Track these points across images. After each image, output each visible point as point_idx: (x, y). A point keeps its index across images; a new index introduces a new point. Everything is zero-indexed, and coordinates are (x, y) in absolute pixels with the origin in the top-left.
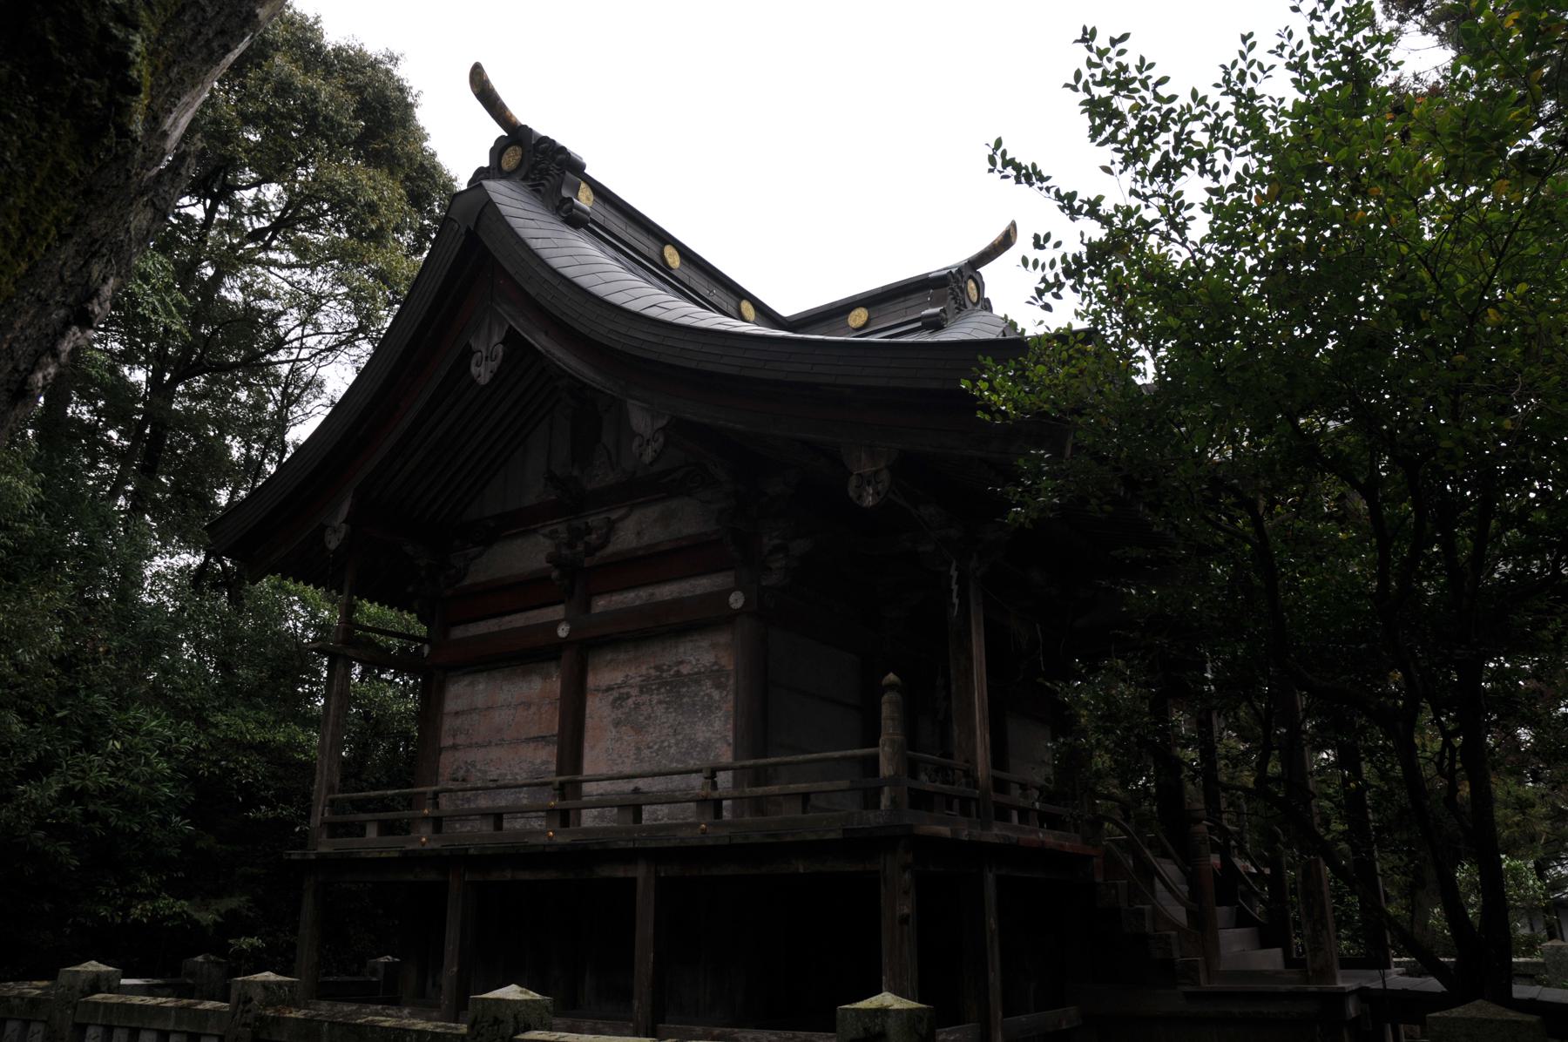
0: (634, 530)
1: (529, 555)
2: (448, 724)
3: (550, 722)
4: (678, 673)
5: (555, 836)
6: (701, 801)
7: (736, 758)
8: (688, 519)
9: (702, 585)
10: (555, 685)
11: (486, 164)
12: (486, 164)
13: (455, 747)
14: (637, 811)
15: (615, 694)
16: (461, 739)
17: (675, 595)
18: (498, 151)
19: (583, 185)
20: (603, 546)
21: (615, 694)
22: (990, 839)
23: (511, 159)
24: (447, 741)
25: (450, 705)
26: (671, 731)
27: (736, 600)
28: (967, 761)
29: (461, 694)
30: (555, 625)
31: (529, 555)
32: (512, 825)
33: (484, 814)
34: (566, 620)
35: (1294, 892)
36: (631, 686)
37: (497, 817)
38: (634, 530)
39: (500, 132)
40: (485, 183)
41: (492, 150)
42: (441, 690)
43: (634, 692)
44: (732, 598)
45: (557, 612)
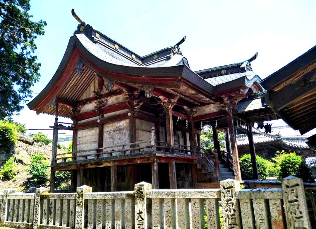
0: (112, 100)
1: (90, 107)
2: (78, 140)
3: (97, 138)
4: (120, 128)
5: (220, 217)
6: (122, 151)
7: (256, 144)
8: (121, 98)
9: (124, 111)
10: (210, 93)
11: (77, 30)
12: (77, 30)
13: (80, 144)
14: (111, 154)
15: (109, 132)
16: (81, 143)
17: (115, 114)
18: (79, 27)
19: (96, 33)
20: (105, 105)
21: (109, 132)
22: (174, 156)
23: (82, 29)
24: (78, 143)
25: (78, 136)
26: (119, 139)
27: (129, 114)
28: (169, 142)
29: (80, 133)
30: (97, 120)
31: (90, 107)
32: (89, 157)
33: (84, 156)
34: (99, 119)
35: (165, 155)
36: (112, 131)
37: (86, 157)
38: (112, 100)
39: (79, 23)
40: (76, 35)
41: (78, 27)
42: (77, 133)
43: (112, 132)
44: (129, 114)
45: (97, 118)
